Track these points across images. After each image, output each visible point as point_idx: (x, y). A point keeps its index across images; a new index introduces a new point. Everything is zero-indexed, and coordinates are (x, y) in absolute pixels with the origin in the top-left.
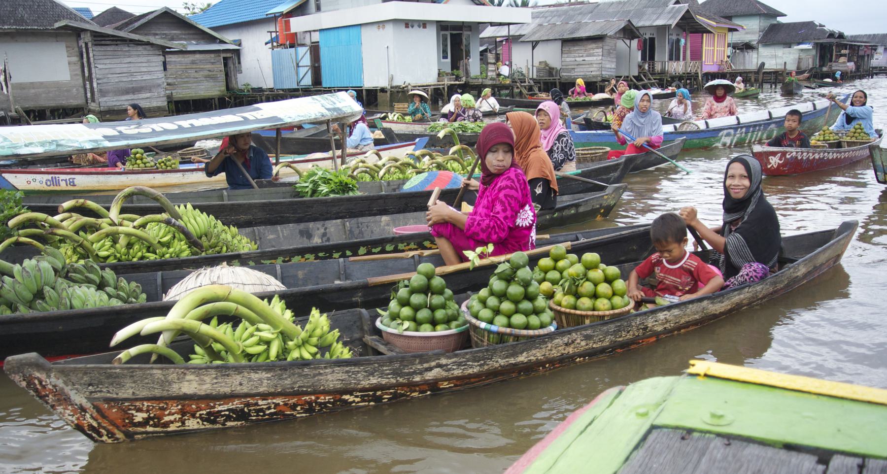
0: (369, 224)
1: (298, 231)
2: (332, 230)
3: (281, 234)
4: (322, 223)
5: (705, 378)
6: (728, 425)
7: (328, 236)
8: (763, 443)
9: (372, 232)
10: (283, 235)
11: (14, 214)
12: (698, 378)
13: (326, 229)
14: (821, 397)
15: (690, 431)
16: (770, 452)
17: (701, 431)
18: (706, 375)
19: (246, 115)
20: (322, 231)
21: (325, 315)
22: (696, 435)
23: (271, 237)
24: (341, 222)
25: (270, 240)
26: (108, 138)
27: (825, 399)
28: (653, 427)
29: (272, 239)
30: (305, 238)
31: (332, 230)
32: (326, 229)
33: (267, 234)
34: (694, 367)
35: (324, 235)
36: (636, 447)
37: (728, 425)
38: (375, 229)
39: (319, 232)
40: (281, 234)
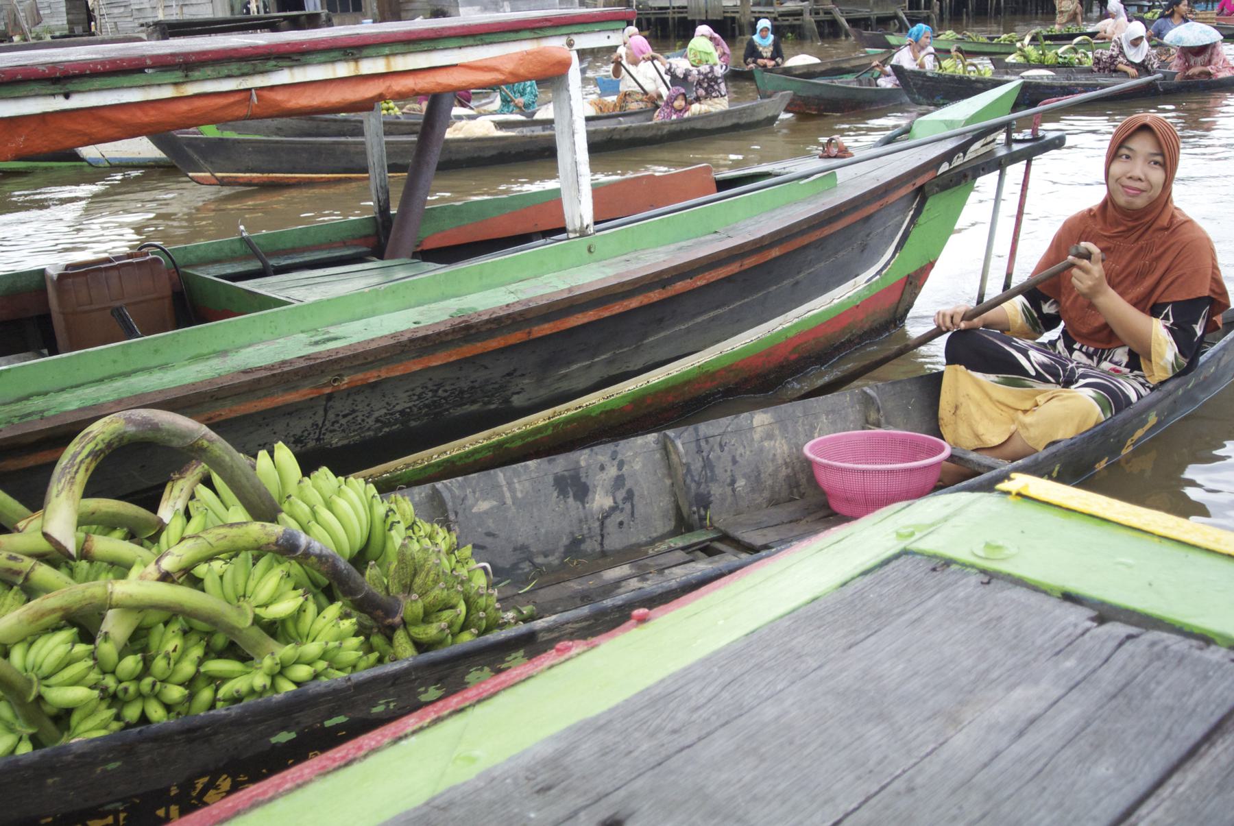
0: (726, 440)
1: (551, 479)
2: (637, 466)
3: (508, 494)
4: (610, 447)
5: (1019, 498)
6: (1003, 559)
7: (629, 484)
8: (1035, 588)
9: (735, 462)
10: (514, 498)
11: (27, 220)
12: (1009, 497)
13: (621, 465)
14: (1164, 541)
15: (948, 562)
16: (1034, 599)
17: (964, 565)
18: (1019, 494)
19: (466, 695)
20: (613, 471)
21: (461, 10)
22: (954, 567)
23: (484, 506)
24: (657, 442)
25: (482, 516)
26: (89, 53)
27: (1169, 544)
28: (905, 553)
29: (486, 512)
30: (571, 500)
31: (637, 466)
32: (621, 465)
33: (470, 501)
34: (1011, 482)
35: (619, 481)
36: (865, 573)
37: (1003, 559)
38: (741, 450)
39: (603, 475)
40: (508, 494)
